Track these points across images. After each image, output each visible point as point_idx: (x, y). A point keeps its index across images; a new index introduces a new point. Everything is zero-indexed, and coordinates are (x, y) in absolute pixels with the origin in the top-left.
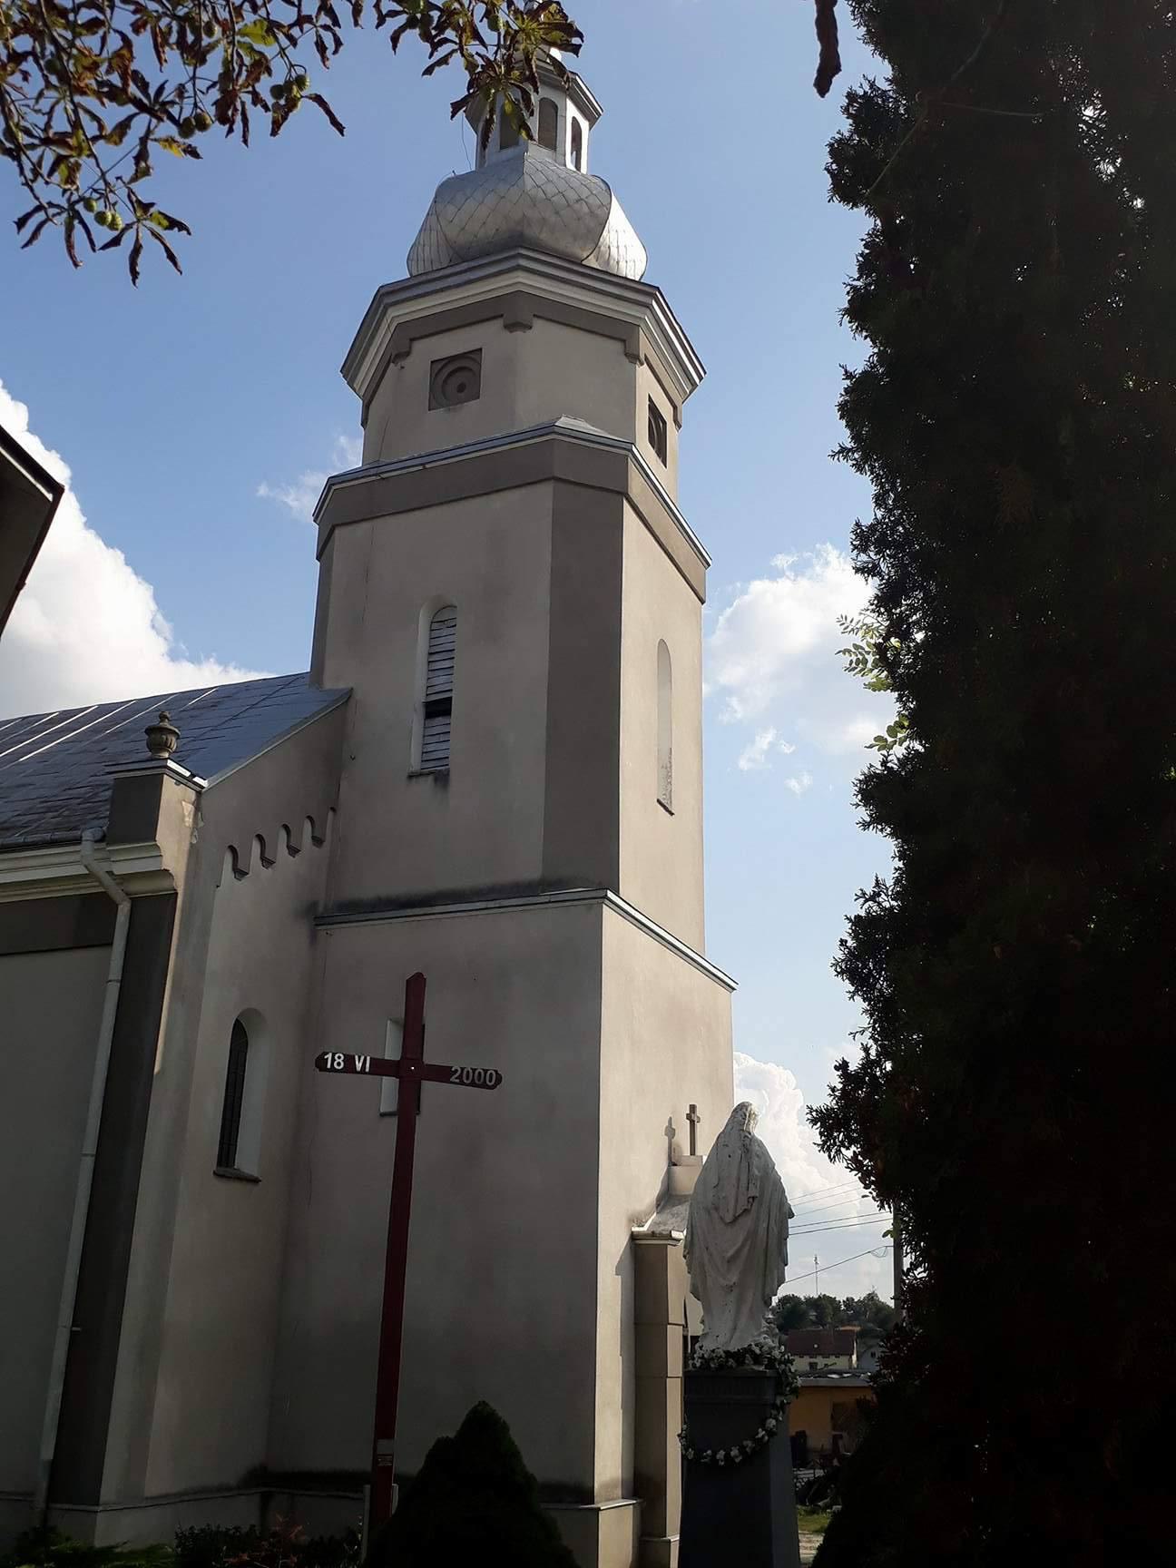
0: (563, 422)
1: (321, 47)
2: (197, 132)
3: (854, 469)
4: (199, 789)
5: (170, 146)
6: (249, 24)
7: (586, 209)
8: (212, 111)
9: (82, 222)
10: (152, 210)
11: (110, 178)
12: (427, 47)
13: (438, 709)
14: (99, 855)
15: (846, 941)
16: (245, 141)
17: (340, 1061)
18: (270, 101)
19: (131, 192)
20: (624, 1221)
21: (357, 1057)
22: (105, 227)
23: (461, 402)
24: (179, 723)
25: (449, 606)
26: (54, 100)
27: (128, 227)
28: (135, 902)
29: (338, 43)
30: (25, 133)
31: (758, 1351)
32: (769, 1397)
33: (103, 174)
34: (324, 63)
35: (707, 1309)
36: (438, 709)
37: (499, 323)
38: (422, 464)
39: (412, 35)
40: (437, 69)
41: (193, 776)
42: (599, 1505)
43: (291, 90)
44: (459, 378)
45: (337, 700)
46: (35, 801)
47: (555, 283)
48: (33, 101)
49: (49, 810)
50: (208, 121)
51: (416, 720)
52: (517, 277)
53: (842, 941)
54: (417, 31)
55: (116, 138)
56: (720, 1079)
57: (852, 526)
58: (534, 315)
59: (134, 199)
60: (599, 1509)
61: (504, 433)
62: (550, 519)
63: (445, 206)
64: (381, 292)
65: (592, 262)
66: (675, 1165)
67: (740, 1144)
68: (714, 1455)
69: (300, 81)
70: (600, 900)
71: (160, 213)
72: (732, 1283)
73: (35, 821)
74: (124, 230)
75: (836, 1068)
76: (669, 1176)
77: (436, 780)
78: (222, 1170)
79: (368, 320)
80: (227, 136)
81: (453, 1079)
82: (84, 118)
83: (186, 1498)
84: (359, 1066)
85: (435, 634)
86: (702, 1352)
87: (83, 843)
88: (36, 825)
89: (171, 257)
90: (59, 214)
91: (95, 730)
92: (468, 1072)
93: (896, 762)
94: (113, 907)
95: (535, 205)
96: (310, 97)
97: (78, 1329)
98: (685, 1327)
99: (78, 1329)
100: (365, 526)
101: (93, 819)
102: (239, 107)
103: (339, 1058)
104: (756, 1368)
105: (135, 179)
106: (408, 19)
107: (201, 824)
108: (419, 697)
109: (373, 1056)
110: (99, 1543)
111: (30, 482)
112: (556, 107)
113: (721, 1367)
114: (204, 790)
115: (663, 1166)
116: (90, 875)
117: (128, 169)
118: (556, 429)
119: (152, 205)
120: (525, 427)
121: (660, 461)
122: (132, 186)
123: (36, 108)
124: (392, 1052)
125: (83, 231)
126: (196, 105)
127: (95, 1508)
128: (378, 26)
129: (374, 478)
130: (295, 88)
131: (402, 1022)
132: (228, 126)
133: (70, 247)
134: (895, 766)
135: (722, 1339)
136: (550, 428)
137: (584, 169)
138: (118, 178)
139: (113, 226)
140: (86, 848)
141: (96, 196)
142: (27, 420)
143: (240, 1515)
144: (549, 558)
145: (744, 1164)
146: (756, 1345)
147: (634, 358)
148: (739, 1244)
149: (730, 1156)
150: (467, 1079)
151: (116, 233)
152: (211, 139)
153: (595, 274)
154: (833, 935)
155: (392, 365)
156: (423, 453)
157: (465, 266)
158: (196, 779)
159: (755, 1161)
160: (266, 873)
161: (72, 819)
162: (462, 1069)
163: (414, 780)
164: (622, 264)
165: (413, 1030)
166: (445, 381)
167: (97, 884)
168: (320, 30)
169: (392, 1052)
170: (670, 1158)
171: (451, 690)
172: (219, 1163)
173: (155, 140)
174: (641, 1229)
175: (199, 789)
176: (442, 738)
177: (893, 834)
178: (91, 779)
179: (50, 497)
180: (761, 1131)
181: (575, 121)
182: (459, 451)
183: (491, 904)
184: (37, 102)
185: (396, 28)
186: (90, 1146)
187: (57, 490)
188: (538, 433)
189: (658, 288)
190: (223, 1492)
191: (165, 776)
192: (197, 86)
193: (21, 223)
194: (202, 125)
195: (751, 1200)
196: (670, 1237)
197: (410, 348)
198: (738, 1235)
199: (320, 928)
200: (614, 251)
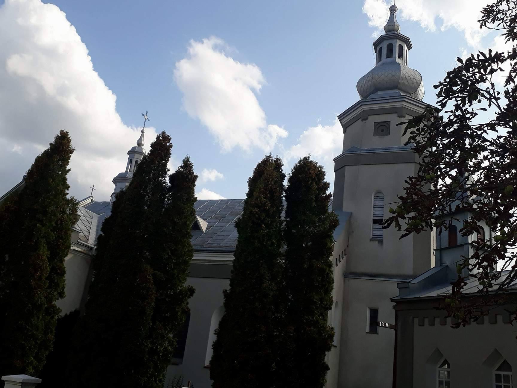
7: (415, 81)
38: (374, 152)
58: (406, 114)
84: (387, 326)
100: (357, 166)
108: (372, 218)
142: (59, 9)
163: (372, 241)
197: (368, 118)
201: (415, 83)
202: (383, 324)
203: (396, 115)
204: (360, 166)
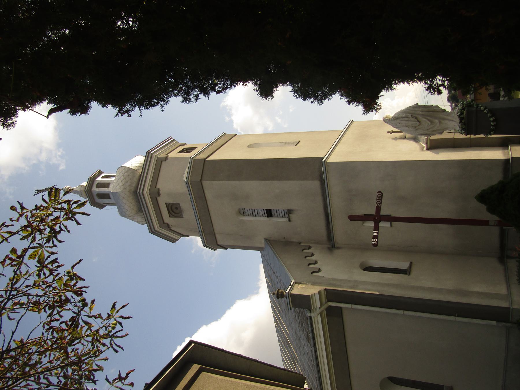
0: (185, 178)
2: (86, 302)
3: (168, 104)
4: (295, 283)
5: (92, 308)
6: (58, 285)
8: (80, 297)
9: (115, 333)
10: (110, 313)
12: (62, 232)
13: (269, 213)
14: (315, 310)
15: (312, 101)
17: (374, 240)
18: (74, 281)
20: (423, 152)
21: (374, 235)
23: (181, 208)
24: (276, 289)
25: (239, 211)
26: (84, 341)
27: (115, 320)
28: (328, 300)
30: (94, 349)
31: (459, 113)
32: (474, 109)
34: (63, 266)
36: (269, 213)
37: (158, 198)
38: (199, 219)
39: (59, 237)
40: (68, 229)
41: (291, 285)
42: (510, 157)
45: (268, 243)
46: (300, 329)
47: (146, 182)
48: (84, 346)
49: (302, 325)
50: (83, 298)
52: (145, 193)
53: (311, 103)
54: (58, 235)
55: (89, 325)
57: (183, 104)
58: (156, 188)
59: (107, 319)
60: (512, 157)
61: (189, 196)
62: (212, 181)
63: (127, 214)
64: (151, 232)
65: (140, 171)
66: (406, 137)
67: (396, 121)
69: (69, 273)
70: (326, 163)
71: (111, 311)
72: (438, 122)
73: (305, 329)
75: (349, 104)
76: (409, 139)
77: (290, 213)
78: (408, 273)
79: (159, 236)
80: (87, 293)
81: (380, 206)
82: (87, 334)
83: (508, 281)
84: (376, 234)
85: (247, 215)
86: (460, 131)
87: (311, 316)
88: (307, 329)
89: (123, 307)
90: (113, 340)
91: (279, 312)
92: (378, 201)
93: (256, 87)
94: (330, 307)
95: (125, 189)
97: (456, 314)
99: (456, 314)
100: (217, 236)
101: (304, 313)
102: (78, 289)
103: (373, 240)
104: (465, 114)
105: (102, 318)
106: (54, 238)
107: (305, 282)
108: (266, 219)
109: (373, 230)
111: (188, 351)
112: (99, 183)
113: (464, 124)
114: (295, 282)
115: (405, 141)
116: (321, 314)
117: (99, 320)
118: (187, 180)
119: (108, 314)
120: (187, 189)
121: (196, 149)
122: (104, 318)
123: (86, 345)
124: (372, 224)
126: (78, 302)
127: (511, 309)
128: (57, 247)
129: (203, 233)
130: (70, 274)
131: (363, 221)
132: (83, 293)
133: (122, 337)
134: (258, 87)
135: (456, 124)
137: (115, 174)
138: (102, 323)
139: (115, 324)
140: (312, 315)
141: (107, 329)
144: (224, 182)
145: (402, 119)
146: (458, 114)
147: (166, 158)
148: (426, 120)
149: (399, 124)
150: (380, 201)
151: (118, 323)
152: (88, 297)
153: (143, 170)
155: (171, 229)
156: (195, 219)
157: (143, 208)
158: (292, 284)
159: (401, 116)
160: (319, 263)
161: (304, 319)
162: (377, 203)
163: (291, 220)
164: (141, 162)
165: (365, 218)
167: (323, 312)
168: (53, 267)
169: (372, 224)
170: (403, 139)
171: (264, 209)
172: (406, 274)
173: (90, 312)
174: (425, 147)
175: (295, 283)
176: (278, 211)
177: (276, 87)
178: (293, 313)
179: (193, 344)
181: (102, 178)
183: (327, 196)
184: (85, 345)
185: (57, 241)
186: (400, 312)
187: (191, 342)
188: (188, 185)
191: (291, 293)
192: (73, 302)
193: (116, 351)
194: (84, 300)
195: (413, 117)
197: (166, 223)
198: (423, 120)
199: (335, 246)
200: (137, 165)
201: (128, 173)
202: (374, 240)
203: (158, 198)
204: (216, 232)
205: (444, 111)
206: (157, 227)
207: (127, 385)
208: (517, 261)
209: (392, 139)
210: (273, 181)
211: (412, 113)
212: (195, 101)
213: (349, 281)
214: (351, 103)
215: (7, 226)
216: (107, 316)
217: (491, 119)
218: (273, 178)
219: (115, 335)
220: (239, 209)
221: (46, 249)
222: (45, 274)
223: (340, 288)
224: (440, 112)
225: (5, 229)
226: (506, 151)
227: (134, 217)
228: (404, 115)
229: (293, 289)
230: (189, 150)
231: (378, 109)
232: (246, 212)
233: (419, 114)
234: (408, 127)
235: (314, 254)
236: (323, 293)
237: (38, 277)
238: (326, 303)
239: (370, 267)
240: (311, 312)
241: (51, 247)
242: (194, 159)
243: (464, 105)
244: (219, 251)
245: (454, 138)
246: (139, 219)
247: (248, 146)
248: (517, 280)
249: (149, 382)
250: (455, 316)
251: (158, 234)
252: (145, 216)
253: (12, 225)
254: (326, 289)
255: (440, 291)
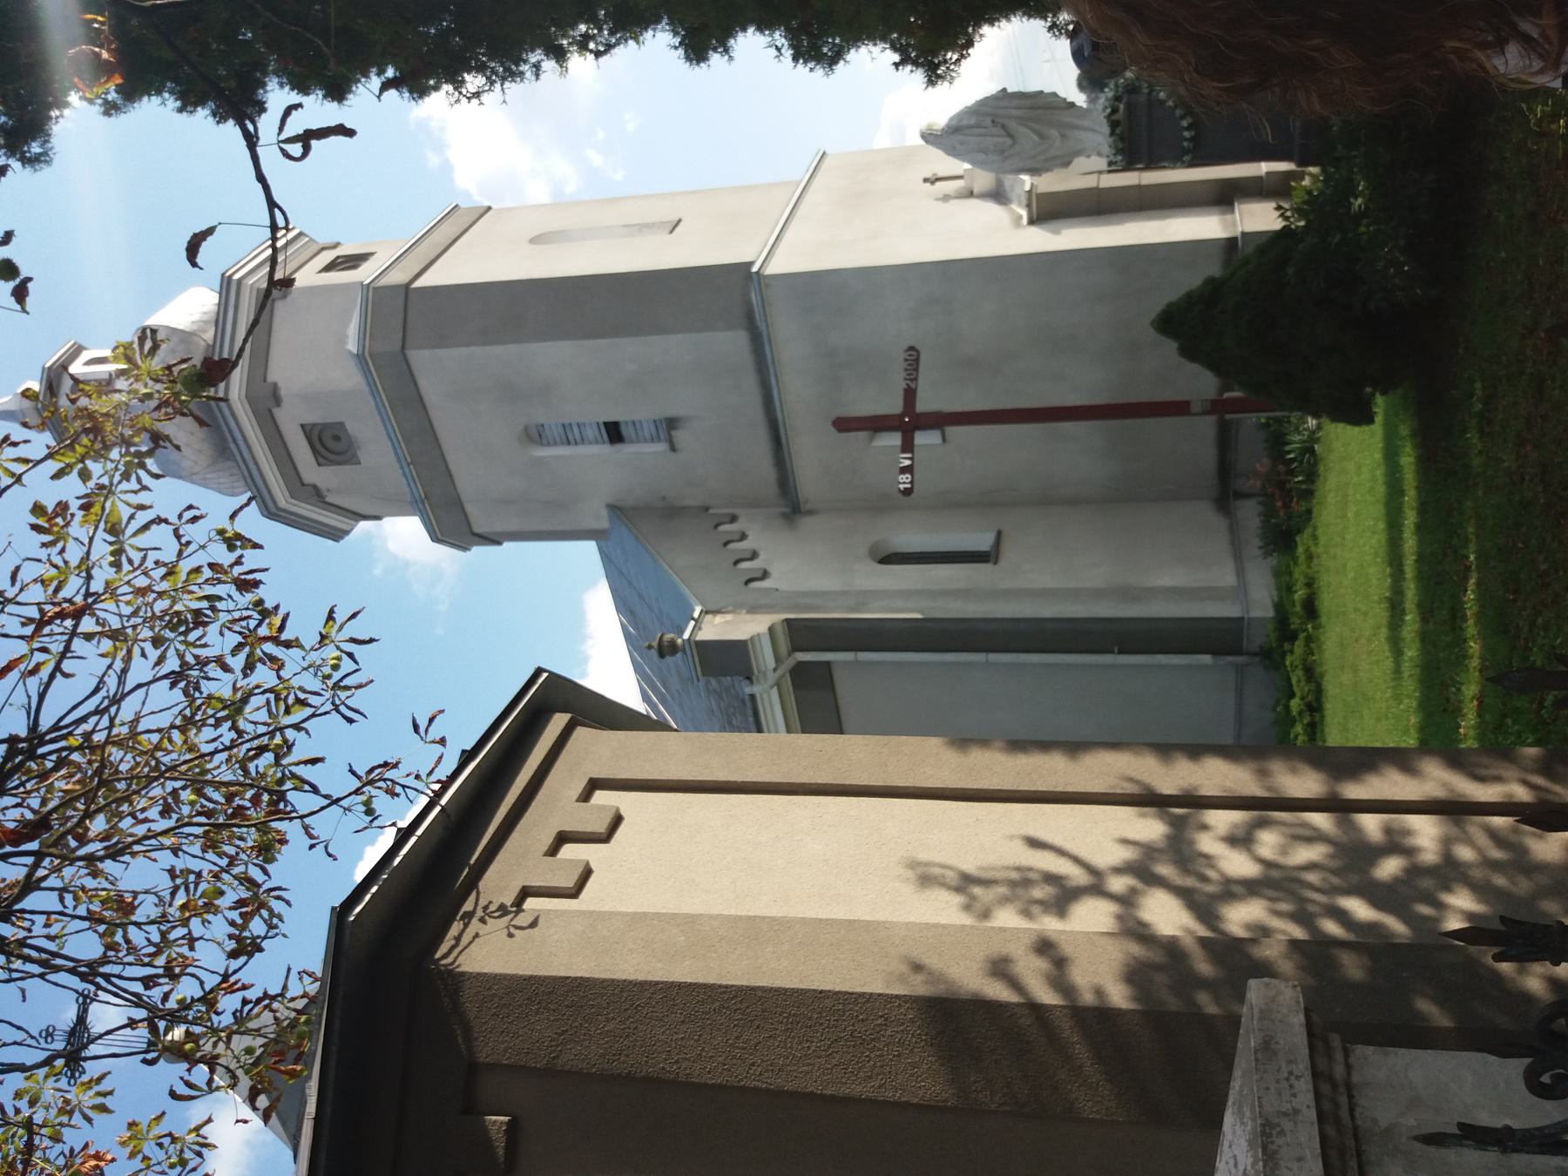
0: (352, 346)
1: (194, 519)
9: (341, 680)
10: (324, 633)
11: (305, 664)
13: (614, 433)
16: (267, 570)
19: (312, 649)
22: (342, 664)
23: (348, 435)
27: (338, 648)
28: (795, 648)
29: (190, 507)
31: (1109, 110)
32: (1142, 99)
33: (304, 669)
35: (1078, 153)
36: (614, 433)
37: (276, 411)
38: (408, 464)
41: (693, 619)
43: (229, 538)
44: (331, 444)
51: (626, 450)
56: (899, 158)
68: (1187, 139)
69: (221, 532)
74: (342, 651)
75: (897, 69)
77: (674, 428)
81: (913, 386)
84: (908, 463)
89: (354, 616)
91: (663, 702)
94: (800, 664)
96: (232, 524)
98: (1100, 172)
100: (470, 509)
107: (730, 608)
108: (606, 449)
109: (899, 449)
110: (1271, 613)
113: (1122, 138)
116: (778, 684)
117: (294, 652)
118: (360, 352)
119: (320, 633)
122: (308, 648)
125: (348, 678)
127: (1246, 621)
128: (149, 490)
129: (427, 505)
131: (871, 433)
136: (360, 358)
140: (756, 689)
141: (319, 674)
143: (1250, 513)
144: (473, 349)
151: (344, 656)
153: (220, 330)
154: (808, 77)
155: (327, 499)
157: (232, 446)
158: (696, 615)
159: (965, 122)
160: (762, 556)
163: (676, 447)
165: (877, 424)
166: (331, 452)
172: (987, 561)
176: (638, 425)
178: (702, 694)
180: (941, 120)
182: (392, 435)
183: (772, 371)
189: (223, 275)
190: (1234, 529)
193: (350, 721)
194: (260, 602)
196: (1030, 192)
197: (309, 485)
198: (1022, 132)
205: (1072, 105)
206: (282, 499)
207: (433, 742)
208: (1259, 503)
209: (937, 199)
210: (617, 340)
211: (991, 115)
212: (534, 78)
213: (844, 593)
214: (901, 68)
215: (15, 444)
216: (319, 638)
217: (1185, 123)
218: (617, 331)
219: (342, 684)
220: (526, 428)
221: (123, 496)
222: (130, 562)
223: (824, 612)
224: (1060, 108)
225: (10, 452)
226: (1229, 217)
227: (208, 476)
228: (973, 121)
229: (700, 629)
230: (354, 261)
231: (952, 78)
232: (548, 432)
233: (1010, 117)
234: (984, 151)
235: (748, 533)
236: (780, 631)
237: (115, 569)
238: (789, 655)
239: (896, 554)
240: (752, 683)
241: (135, 492)
242: (374, 288)
243: (1120, 89)
244: (478, 551)
245: (1097, 189)
246: (222, 480)
247: (533, 241)
248: (1260, 548)
249: (468, 748)
250: (1111, 652)
251: (290, 520)
252: (243, 467)
253: (26, 442)
254: (787, 620)
255: (1075, 594)
